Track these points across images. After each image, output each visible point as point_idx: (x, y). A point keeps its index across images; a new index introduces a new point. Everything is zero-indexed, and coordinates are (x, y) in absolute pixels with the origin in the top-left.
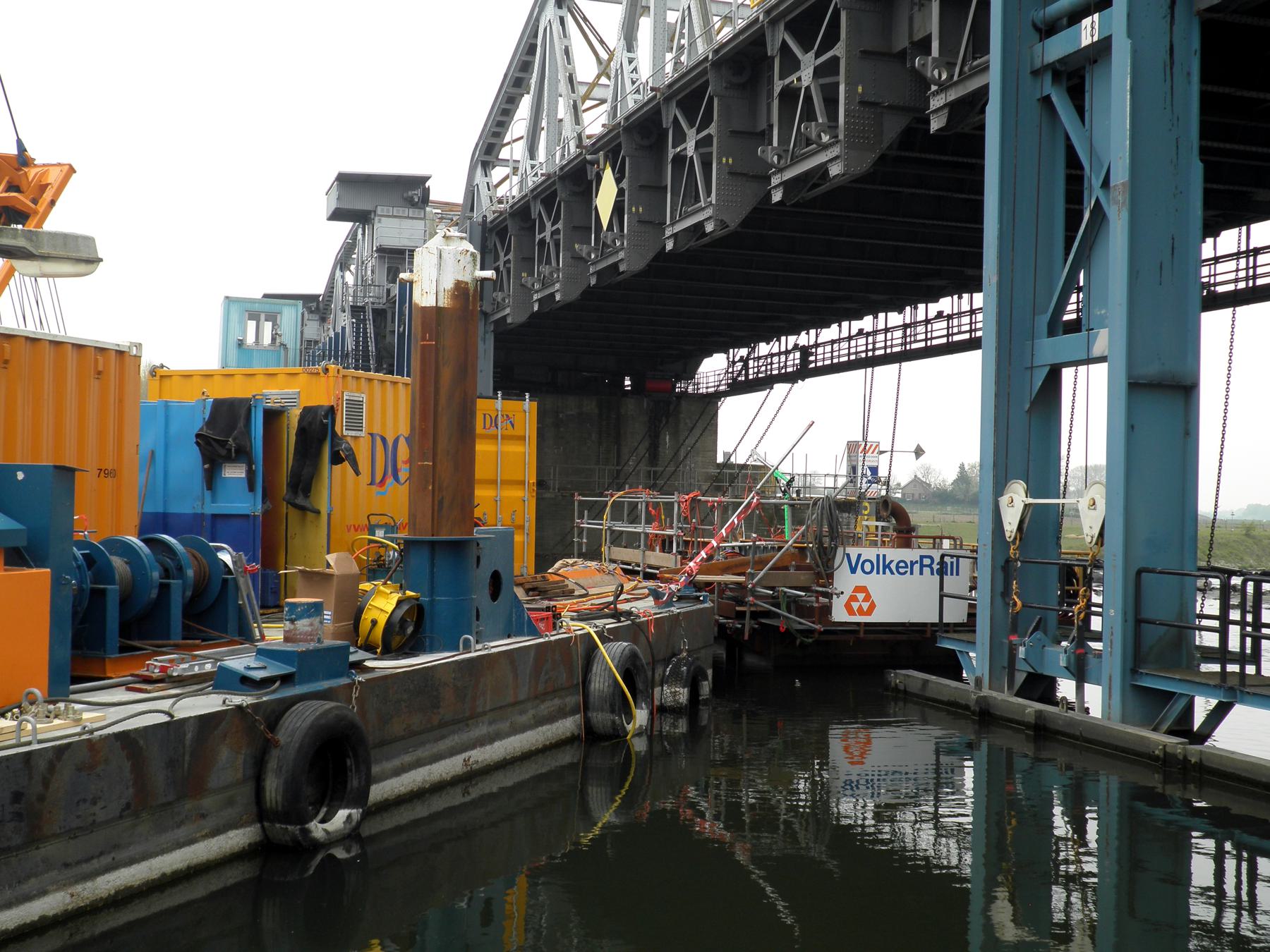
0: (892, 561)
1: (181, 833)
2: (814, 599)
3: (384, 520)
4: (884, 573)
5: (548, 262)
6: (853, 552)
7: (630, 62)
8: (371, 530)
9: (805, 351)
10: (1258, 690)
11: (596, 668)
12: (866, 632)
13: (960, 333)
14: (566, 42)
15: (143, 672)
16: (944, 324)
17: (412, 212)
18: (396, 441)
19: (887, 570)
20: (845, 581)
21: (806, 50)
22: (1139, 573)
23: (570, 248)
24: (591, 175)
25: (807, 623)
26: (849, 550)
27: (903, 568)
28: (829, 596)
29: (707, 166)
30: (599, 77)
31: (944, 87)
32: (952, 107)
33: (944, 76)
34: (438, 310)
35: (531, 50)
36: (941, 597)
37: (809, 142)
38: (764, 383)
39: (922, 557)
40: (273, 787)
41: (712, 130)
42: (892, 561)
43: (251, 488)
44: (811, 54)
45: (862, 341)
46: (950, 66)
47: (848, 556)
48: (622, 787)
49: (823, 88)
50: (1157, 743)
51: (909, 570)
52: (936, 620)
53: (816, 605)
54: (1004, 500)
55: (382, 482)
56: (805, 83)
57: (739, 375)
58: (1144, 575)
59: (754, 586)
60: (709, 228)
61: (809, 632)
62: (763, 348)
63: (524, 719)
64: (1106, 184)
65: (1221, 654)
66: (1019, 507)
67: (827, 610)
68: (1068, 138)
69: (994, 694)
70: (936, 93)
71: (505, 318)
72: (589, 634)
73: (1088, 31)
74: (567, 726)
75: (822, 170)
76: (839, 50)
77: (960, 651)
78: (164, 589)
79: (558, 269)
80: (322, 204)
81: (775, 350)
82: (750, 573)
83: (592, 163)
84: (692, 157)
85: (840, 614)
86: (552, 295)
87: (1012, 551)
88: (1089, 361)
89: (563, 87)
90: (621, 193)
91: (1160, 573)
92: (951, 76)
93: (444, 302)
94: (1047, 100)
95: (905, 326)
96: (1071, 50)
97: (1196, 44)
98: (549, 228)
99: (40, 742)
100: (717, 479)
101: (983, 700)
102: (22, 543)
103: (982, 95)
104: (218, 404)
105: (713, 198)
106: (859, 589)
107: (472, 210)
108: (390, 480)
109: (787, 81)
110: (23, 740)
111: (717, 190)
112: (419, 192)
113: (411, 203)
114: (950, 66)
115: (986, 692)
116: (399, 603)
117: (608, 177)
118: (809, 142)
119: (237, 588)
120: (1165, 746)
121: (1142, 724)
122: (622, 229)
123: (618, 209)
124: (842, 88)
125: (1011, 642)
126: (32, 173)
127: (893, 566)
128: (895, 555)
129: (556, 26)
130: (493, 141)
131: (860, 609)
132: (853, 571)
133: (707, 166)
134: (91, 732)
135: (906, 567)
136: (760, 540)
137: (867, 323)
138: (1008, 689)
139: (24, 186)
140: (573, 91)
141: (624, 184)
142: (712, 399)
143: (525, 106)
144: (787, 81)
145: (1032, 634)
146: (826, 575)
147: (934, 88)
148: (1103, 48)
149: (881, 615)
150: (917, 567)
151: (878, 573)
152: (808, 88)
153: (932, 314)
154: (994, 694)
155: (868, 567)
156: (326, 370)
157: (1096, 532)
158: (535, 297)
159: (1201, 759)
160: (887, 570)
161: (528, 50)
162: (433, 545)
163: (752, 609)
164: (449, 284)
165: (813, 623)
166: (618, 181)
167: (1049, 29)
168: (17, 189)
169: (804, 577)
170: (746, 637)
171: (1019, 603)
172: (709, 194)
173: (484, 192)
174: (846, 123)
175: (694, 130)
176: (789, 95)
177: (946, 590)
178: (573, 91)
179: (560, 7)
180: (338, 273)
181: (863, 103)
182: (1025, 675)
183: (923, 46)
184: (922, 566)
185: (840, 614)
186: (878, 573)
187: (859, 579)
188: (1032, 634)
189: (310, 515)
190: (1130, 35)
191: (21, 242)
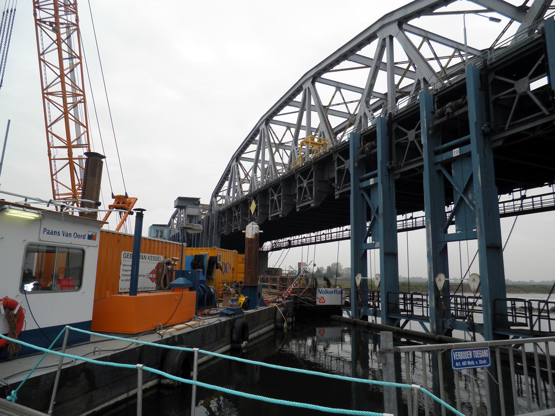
1: (221, 345)
3: (226, 281)
5: (237, 221)
6: (321, 289)
7: (255, 176)
8: (223, 284)
9: (289, 241)
11: (277, 314)
13: (328, 238)
14: (238, 170)
15: (203, 313)
16: (325, 236)
17: (195, 207)
18: (226, 264)
20: (319, 295)
21: (305, 179)
22: (388, 293)
23: (242, 218)
24: (249, 201)
26: (319, 289)
27: (331, 292)
28: (315, 299)
29: (280, 202)
30: (245, 178)
31: (338, 190)
32: (341, 194)
33: (338, 188)
34: (252, 239)
35: (229, 171)
36: (342, 299)
37: (306, 198)
38: (279, 249)
39: (335, 290)
40: (234, 336)
41: (281, 194)
43: (204, 274)
44: (306, 180)
45: (305, 239)
46: (340, 186)
47: (319, 290)
48: (283, 340)
49: (309, 187)
50: (395, 329)
52: (341, 304)
54: (356, 278)
55: (224, 273)
56: (305, 186)
57: (274, 247)
58: (389, 294)
60: (280, 216)
61: (312, 307)
62: (280, 241)
63: (266, 324)
64: (377, 212)
65: (404, 310)
67: (315, 302)
68: (367, 201)
69: (357, 320)
70: (336, 191)
71: (224, 233)
72: (276, 306)
73: (372, 182)
74: (272, 326)
75: (309, 205)
76: (313, 180)
78: (204, 295)
79: (239, 223)
80: (173, 204)
81: (283, 241)
83: (249, 199)
84: (276, 200)
85: (318, 303)
86: (238, 229)
88: (375, 248)
89: (237, 180)
90: (257, 206)
91: (393, 293)
92: (340, 188)
93: (253, 237)
94: (362, 195)
95: (315, 236)
96: (368, 185)
97: (394, 186)
98: (237, 213)
99: (204, 325)
100: (267, 271)
101: (355, 321)
102: (191, 286)
103: (349, 192)
104: (196, 256)
105: (281, 208)
106: (322, 297)
107: (212, 207)
108: (225, 272)
109: (300, 185)
110: (200, 325)
111: (283, 206)
112: (198, 202)
113: (195, 204)
114: (340, 186)
115: (354, 319)
116: (246, 299)
117: (254, 203)
118: (306, 198)
119: (214, 296)
121: (391, 325)
122: (257, 214)
123: (256, 210)
124: (314, 188)
125: (359, 309)
126: (128, 199)
128: (329, 290)
129: (236, 167)
130: (218, 191)
131: (322, 302)
132: (320, 293)
133: (280, 202)
134: (211, 324)
137: (305, 235)
139: (126, 203)
140: (240, 181)
141: (258, 205)
142: (268, 252)
143: (227, 183)
144: (300, 185)
146: (315, 294)
147: (336, 190)
148: (376, 185)
149: (326, 304)
150: (334, 292)
152: (305, 187)
153: (321, 234)
154: (357, 320)
155: (323, 292)
156: (215, 249)
157: (476, 287)
158: (233, 229)
161: (228, 171)
162: (250, 287)
164: (254, 233)
166: (256, 204)
167: (362, 180)
168: (125, 203)
169: (310, 295)
170: (298, 308)
172: (280, 207)
173: (215, 202)
174: (315, 195)
175: (276, 194)
176: (301, 189)
177: (343, 297)
178: (240, 181)
179: (237, 162)
180: (172, 219)
181: (319, 191)
182: (362, 316)
183: (333, 180)
184: (335, 292)
185: (318, 303)
187: (322, 295)
189: (211, 280)
190: (382, 184)
191: (191, 227)
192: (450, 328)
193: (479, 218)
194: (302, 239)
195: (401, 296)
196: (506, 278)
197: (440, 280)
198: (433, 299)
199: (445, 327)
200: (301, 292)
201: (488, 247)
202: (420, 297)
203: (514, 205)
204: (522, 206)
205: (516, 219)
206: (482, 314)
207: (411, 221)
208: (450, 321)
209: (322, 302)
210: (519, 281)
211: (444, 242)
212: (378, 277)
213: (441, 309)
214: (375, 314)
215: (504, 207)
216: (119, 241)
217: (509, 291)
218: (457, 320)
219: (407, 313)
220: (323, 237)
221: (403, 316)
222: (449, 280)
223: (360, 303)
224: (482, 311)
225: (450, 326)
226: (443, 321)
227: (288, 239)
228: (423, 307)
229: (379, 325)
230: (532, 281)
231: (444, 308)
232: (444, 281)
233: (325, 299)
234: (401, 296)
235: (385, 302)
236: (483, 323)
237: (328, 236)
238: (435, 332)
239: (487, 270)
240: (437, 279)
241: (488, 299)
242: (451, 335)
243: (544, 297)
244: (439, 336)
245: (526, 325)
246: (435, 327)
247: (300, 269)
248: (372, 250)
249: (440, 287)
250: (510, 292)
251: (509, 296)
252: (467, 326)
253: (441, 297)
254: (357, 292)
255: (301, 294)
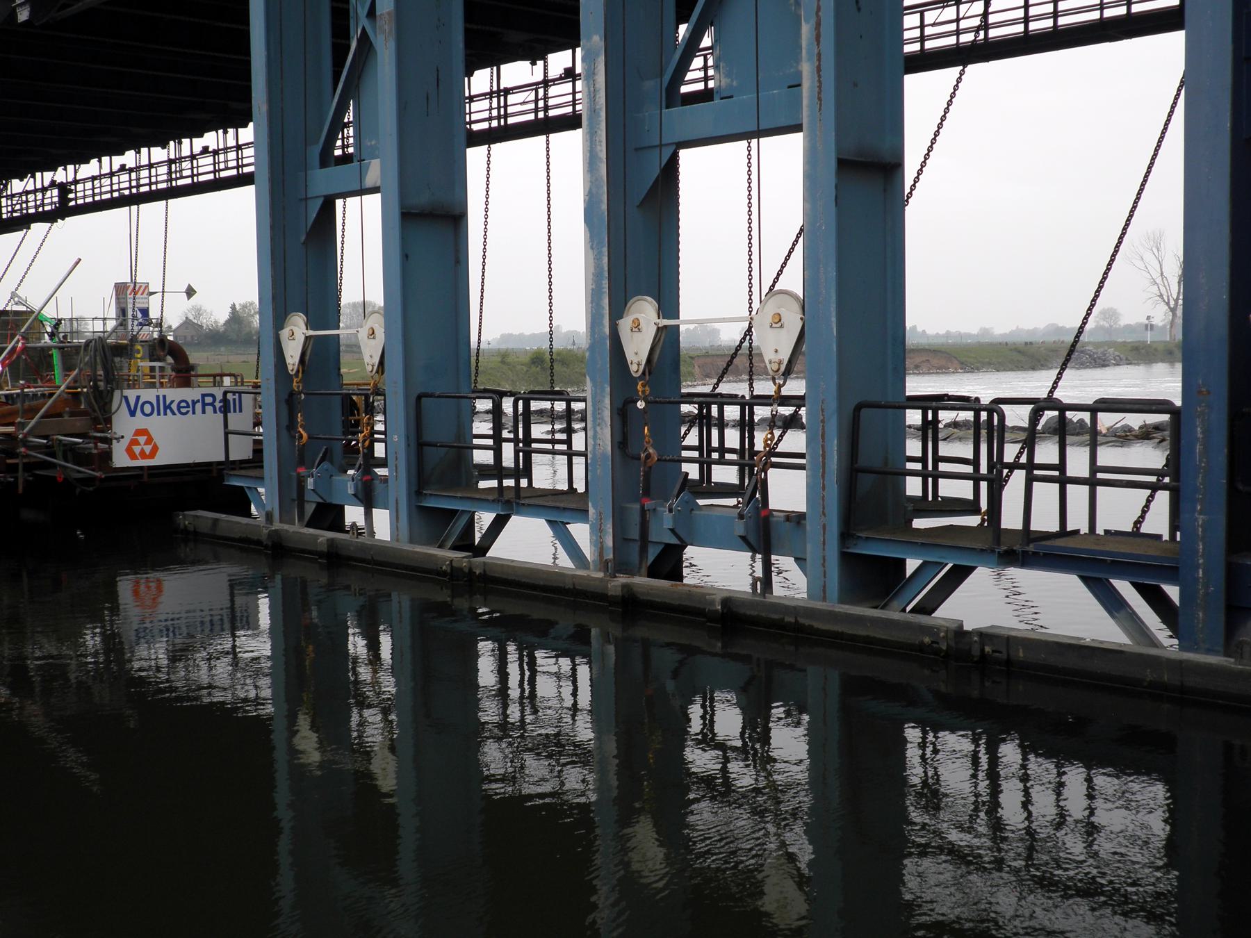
0: (172, 402)
2: (91, 445)
4: (204, 412)
6: (131, 394)
9: (64, 189)
10: (532, 501)
12: (150, 476)
13: (227, 168)
16: (210, 160)
19: (168, 411)
20: (124, 425)
25: (87, 471)
26: (127, 392)
27: (185, 408)
28: (108, 441)
36: (226, 434)
39: (203, 396)
42: (172, 402)
47: (126, 398)
50: (444, 559)
51: (190, 409)
53: (95, 451)
54: (285, 333)
58: (424, 399)
59: (26, 436)
66: (300, 339)
67: (107, 455)
69: (286, 527)
77: (249, 488)
81: (30, 187)
82: (20, 423)
85: (121, 459)
87: (295, 384)
88: (362, 192)
91: (439, 397)
95: (170, 162)
115: (277, 525)
120: (451, 561)
121: (429, 542)
127: (174, 406)
131: (142, 453)
132: (133, 413)
135: (188, 406)
136: (29, 387)
138: (299, 521)
145: (319, 464)
146: (106, 420)
149: (158, 461)
150: (199, 406)
151: (235, 411)
154: (286, 527)
155: (147, 409)
157: (785, 355)
159: (484, 571)
160: (168, 411)
163: (25, 460)
165: (93, 470)
169: (80, 423)
171: (305, 435)
177: (231, 427)
182: (314, 506)
184: (204, 405)
185: (121, 459)
186: (159, 414)
187: (140, 421)
188: (319, 464)
192: (674, 541)
193: (813, 21)
194: (112, 174)
195: (484, 405)
196: (908, 325)
197: (637, 327)
198: (607, 414)
199: (653, 537)
200: (31, 412)
201: (843, 165)
202: (546, 405)
203: (958, 20)
204: (985, 26)
205: (959, 80)
206: (803, 473)
207: (567, 87)
208: (670, 511)
209: (142, 452)
210: (948, 334)
211: (661, 146)
212: (783, 312)
213: (639, 459)
214: (368, 500)
215: (922, 26)
216: (636, 354)
217: (917, 367)
218: (701, 502)
219: (500, 483)
220: (206, 163)
221: (487, 499)
222: (678, 326)
223: (302, 449)
224: (801, 456)
225: (672, 530)
226: (643, 512)
227: (61, 175)
228: (570, 454)
229: (382, 548)
230: (985, 331)
231: (649, 456)
232: (655, 328)
233: (156, 440)
234: (484, 405)
235: (408, 438)
236: (802, 507)
237: (226, 161)
238: (607, 562)
239: (833, 274)
240: (625, 324)
241: (832, 405)
242: (676, 574)
243: (1036, 384)
244: (622, 579)
245: (970, 507)
246: (609, 541)
247: (122, 312)
248: (353, 202)
249: (635, 361)
250: (919, 370)
251: (916, 386)
252: (739, 528)
253: (641, 405)
254: (289, 402)
255: (33, 422)
